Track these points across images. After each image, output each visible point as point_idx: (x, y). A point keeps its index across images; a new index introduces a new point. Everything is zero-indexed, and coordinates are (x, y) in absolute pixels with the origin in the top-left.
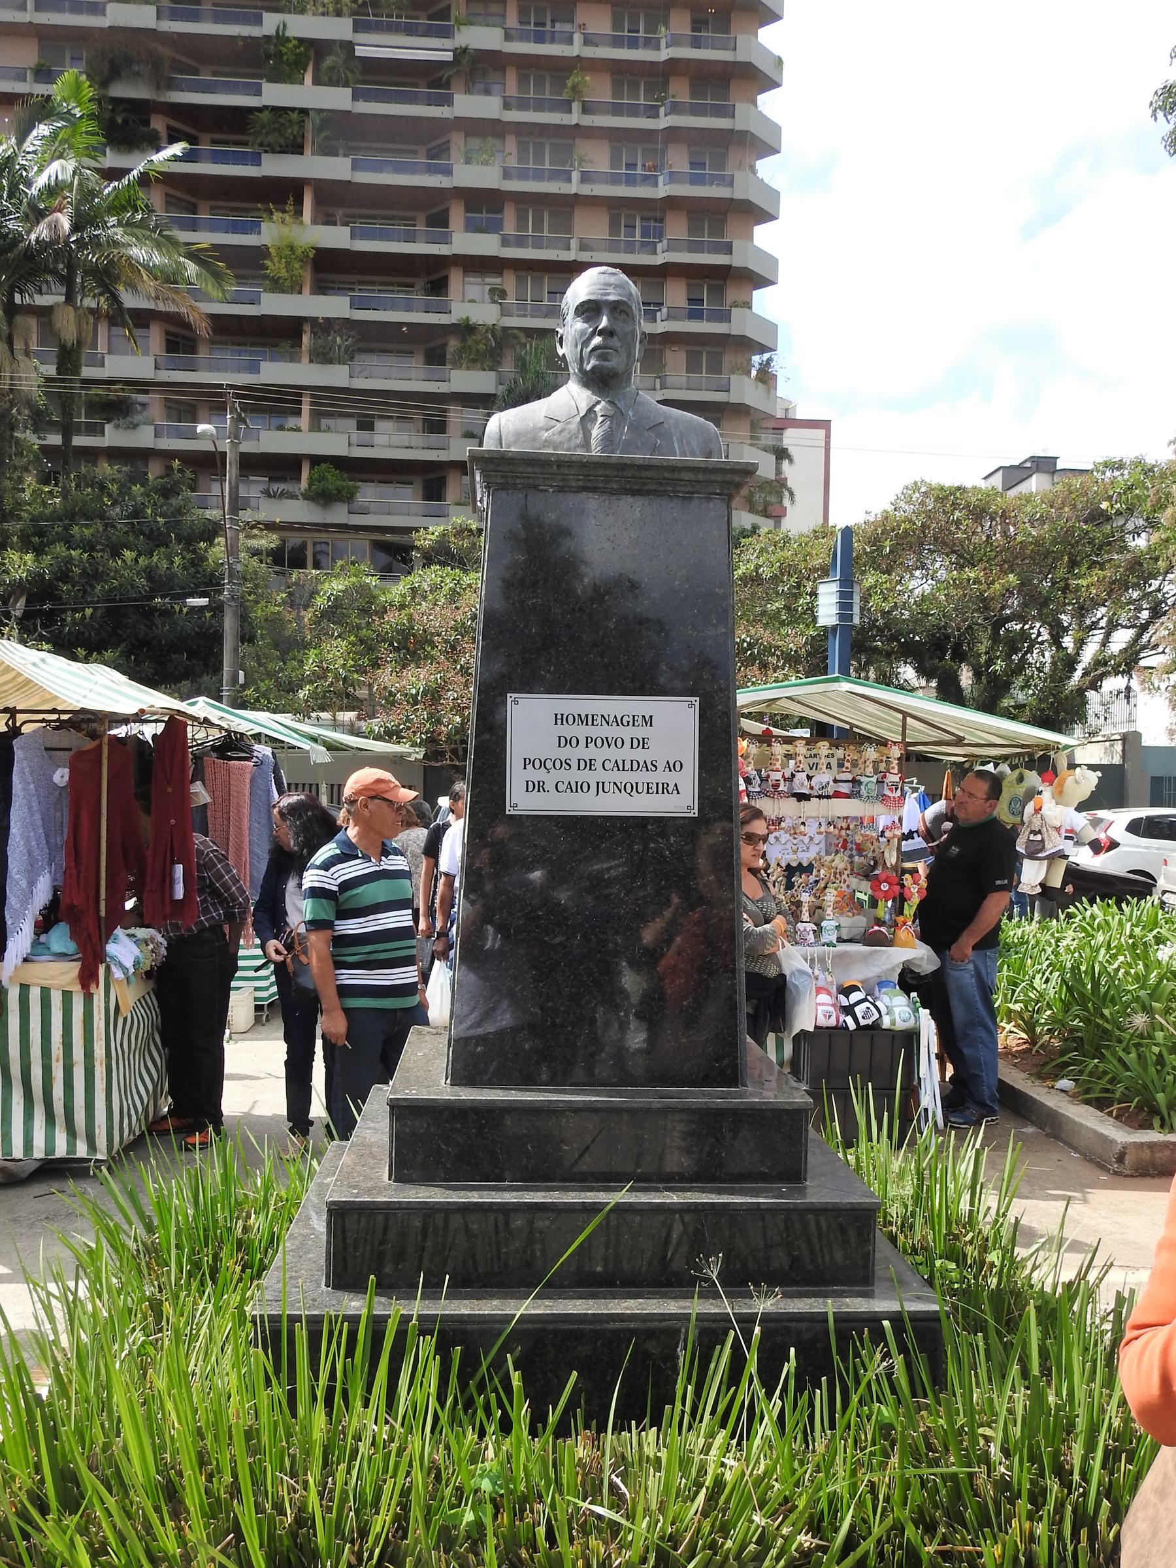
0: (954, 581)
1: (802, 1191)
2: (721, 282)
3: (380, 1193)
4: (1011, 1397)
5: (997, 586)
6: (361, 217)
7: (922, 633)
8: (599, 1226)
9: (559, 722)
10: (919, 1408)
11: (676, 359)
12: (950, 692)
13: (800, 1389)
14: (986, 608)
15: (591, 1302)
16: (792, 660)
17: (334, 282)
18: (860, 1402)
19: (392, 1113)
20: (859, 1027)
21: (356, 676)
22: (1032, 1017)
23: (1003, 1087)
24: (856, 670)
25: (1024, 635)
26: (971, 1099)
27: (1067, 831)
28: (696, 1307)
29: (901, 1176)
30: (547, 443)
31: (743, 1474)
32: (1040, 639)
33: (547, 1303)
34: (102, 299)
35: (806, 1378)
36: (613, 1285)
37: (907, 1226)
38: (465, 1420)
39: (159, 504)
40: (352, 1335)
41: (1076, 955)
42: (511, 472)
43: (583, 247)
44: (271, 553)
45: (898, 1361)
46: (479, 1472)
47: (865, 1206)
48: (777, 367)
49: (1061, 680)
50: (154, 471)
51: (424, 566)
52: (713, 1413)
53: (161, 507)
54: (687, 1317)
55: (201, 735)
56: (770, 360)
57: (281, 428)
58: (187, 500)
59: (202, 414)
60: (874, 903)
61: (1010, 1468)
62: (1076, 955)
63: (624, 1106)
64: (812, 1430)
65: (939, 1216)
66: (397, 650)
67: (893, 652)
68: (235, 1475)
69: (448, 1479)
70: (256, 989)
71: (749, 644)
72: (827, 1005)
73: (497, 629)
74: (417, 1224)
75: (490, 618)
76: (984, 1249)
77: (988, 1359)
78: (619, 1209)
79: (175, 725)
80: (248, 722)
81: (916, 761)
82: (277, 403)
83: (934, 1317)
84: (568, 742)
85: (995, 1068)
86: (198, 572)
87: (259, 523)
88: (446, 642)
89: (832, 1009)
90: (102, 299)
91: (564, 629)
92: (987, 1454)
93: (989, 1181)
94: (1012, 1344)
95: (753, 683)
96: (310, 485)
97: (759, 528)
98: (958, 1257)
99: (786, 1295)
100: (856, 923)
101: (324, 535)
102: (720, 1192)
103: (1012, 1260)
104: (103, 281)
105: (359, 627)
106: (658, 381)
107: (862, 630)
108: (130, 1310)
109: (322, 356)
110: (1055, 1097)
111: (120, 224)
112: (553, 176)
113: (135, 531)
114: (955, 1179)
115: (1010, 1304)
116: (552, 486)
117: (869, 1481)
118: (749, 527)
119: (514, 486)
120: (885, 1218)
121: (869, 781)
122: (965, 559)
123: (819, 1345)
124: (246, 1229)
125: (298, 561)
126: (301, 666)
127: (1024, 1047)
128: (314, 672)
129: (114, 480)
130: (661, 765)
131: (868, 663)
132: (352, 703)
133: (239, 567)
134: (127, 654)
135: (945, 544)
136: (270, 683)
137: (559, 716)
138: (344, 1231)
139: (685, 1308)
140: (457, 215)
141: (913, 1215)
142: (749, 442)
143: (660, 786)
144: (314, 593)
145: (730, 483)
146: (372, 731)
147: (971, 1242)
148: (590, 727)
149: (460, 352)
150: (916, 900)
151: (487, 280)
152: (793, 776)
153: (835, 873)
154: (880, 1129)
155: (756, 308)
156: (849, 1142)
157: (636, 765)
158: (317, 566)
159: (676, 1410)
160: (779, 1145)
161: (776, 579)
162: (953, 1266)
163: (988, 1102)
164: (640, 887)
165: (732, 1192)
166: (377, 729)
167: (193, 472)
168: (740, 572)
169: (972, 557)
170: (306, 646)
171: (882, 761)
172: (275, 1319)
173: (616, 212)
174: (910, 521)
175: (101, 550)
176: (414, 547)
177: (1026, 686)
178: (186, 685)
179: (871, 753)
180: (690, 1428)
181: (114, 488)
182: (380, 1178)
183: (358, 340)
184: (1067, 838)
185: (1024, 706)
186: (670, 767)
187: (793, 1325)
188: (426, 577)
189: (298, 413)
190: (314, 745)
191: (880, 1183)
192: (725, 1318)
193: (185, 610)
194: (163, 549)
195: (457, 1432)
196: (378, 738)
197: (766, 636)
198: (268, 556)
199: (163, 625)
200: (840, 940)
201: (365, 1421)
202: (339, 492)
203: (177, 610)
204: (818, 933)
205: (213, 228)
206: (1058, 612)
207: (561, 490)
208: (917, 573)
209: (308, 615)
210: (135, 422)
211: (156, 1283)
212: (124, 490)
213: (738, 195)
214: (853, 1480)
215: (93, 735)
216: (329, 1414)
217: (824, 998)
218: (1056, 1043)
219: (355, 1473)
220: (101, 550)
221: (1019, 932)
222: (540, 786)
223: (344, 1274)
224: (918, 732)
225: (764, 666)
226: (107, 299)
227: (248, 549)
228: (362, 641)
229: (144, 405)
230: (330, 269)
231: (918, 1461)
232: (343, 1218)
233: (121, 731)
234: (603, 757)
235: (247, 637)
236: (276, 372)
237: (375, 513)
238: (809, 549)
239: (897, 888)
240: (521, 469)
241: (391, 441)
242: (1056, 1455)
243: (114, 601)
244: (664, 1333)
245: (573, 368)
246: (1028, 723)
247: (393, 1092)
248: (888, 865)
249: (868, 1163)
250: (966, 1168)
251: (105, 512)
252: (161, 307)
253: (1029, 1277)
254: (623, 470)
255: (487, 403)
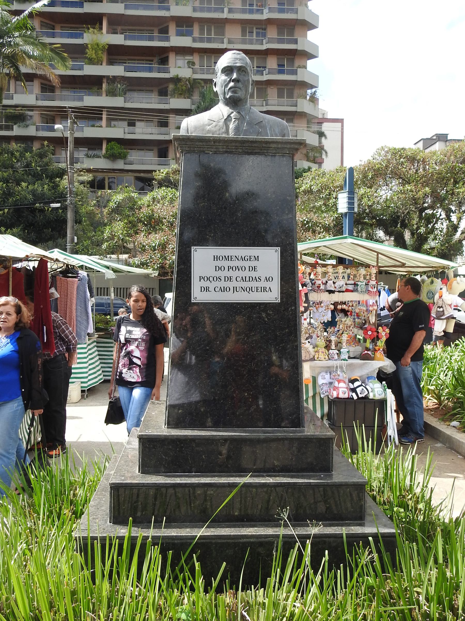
0: (401, 191)
1: (331, 476)
2: (292, 57)
3: (134, 479)
4: (429, 573)
5: (420, 192)
6: (129, 30)
7: (386, 215)
8: (236, 494)
9: (216, 259)
10: (387, 578)
11: (272, 92)
12: (400, 242)
13: (330, 570)
14: (416, 203)
15: (233, 529)
16: (327, 229)
17: (117, 60)
18: (359, 575)
19: (140, 442)
20: (359, 398)
21: (127, 238)
22: (439, 392)
23: (426, 425)
24: (357, 233)
25: (433, 216)
26: (412, 430)
27: (454, 306)
28: (281, 531)
29: (378, 468)
30: (209, 131)
31: (304, 611)
32: (441, 217)
33: (212, 530)
34: (12, 69)
35: (335, 563)
36: (243, 521)
37: (381, 492)
38: (174, 585)
39: (38, 161)
40: (121, 546)
41: (459, 363)
42: (194, 145)
43: (230, 42)
44: (89, 182)
45: (376, 556)
46: (180, 610)
47: (360, 483)
48: (318, 95)
49: (451, 236)
50: (36, 146)
51: (158, 188)
52: (290, 581)
53: (39, 162)
54: (278, 536)
55: (55, 266)
56: (315, 92)
57: (93, 126)
58: (51, 159)
59: (57, 120)
60: (365, 341)
61: (429, 607)
62: (459, 363)
63: (247, 437)
64: (336, 589)
65: (396, 487)
66: (146, 225)
67: (373, 224)
68: (66, 613)
69: (166, 613)
70: (82, 383)
71: (307, 222)
72: (344, 388)
73: (188, 218)
74: (152, 493)
75: (183, 213)
76: (417, 502)
77: (419, 554)
78: (246, 485)
79: (43, 262)
80: (76, 260)
81: (383, 274)
82: (92, 115)
83: (392, 536)
84: (220, 268)
85: (422, 416)
86: (56, 192)
87: (84, 169)
88: (169, 222)
89: (346, 390)
90: (12, 69)
91: (220, 215)
92: (418, 601)
93: (419, 470)
94: (430, 548)
95: (309, 240)
96: (107, 152)
97: (311, 168)
98: (406, 507)
99: (325, 526)
100: (357, 349)
101: (113, 174)
102: (292, 477)
103: (430, 508)
104: (11, 60)
105: (129, 216)
106: (264, 102)
107: (359, 214)
108: (20, 534)
109: (112, 93)
110: (450, 429)
111: (20, 36)
112: (216, 10)
113: (27, 173)
114: (403, 470)
115: (429, 528)
116: (211, 151)
117: (363, 614)
118: (307, 168)
119: (194, 152)
120: (371, 488)
121: (362, 284)
122: (405, 181)
123: (339, 549)
124: (74, 495)
125: (101, 186)
126: (103, 234)
127: (436, 406)
128: (108, 237)
129: (17, 150)
130: (263, 279)
131: (362, 229)
132: (126, 251)
133: (74, 189)
134: (23, 230)
135: (396, 175)
136: (89, 242)
137: (216, 257)
138: (118, 496)
139: (276, 532)
140: (172, 29)
141: (383, 487)
142: (306, 129)
143: (263, 288)
144: (109, 201)
145: (295, 147)
146: (135, 263)
147: (411, 499)
148: (230, 261)
149: (174, 90)
150: (384, 339)
151: (186, 58)
152: (327, 282)
153: (347, 327)
154: (368, 446)
155: (309, 68)
156: (354, 451)
157: (251, 279)
158: (110, 188)
159: (272, 580)
160: (318, 456)
161: (319, 191)
162: (402, 510)
163: (419, 432)
164: (253, 335)
165: (298, 477)
166: (137, 262)
167: (54, 147)
168: (303, 188)
169: (409, 180)
170: (105, 225)
171: (367, 275)
172: (85, 538)
173: (244, 26)
174: (381, 164)
175: (12, 183)
176: (154, 179)
177: (435, 239)
178: (50, 243)
179: (362, 271)
180: (279, 589)
181: (17, 154)
182: (134, 472)
183: (128, 86)
184: (454, 309)
185: (434, 248)
186: (267, 279)
187: (327, 539)
188: (159, 193)
189: (101, 119)
190: (108, 270)
191: (368, 471)
192: (292, 537)
193: (50, 209)
194: (39, 182)
195: (170, 591)
196: (138, 266)
197: (314, 217)
198: (88, 184)
199: (40, 216)
200: (349, 358)
201: (127, 586)
202: (120, 154)
203: (47, 209)
204: (339, 354)
205: (62, 36)
206: (449, 204)
207: (215, 153)
208: (384, 188)
209: (105, 211)
210: (27, 124)
211: (33, 521)
212: (22, 155)
213: (300, 17)
214: (355, 613)
215: (5, 268)
216: (111, 583)
217: (342, 385)
218: (450, 404)
219: (122, 611)
220: (12, 183)
221: (433, 353)
222: (207, 289)
223: (118, 518)
224: (384, 261)
225: (314, 232)
226: (14, 69)
227: (79, 181)
228: (130, 222)
229: (31, 116)
230: (115, 54)
231: (386, 603)
232: (118, 490)
233: (19, 265)
234: (235, 275)
235: (78, 221)
236: (90, 101)
237: (136, 164)
238: (334, 178)
239: (375, 334)
240: (197, 144)
241: (144, 131)
242: (451, 601)
243: (18, 205)
244: (266, 544)
245: (221, 97)
246: (436, 256)
247: (140, 432)
248: (371, 323)
249: (362, 462)
250: (408, 464)
251: (13, 165)
252: (38, 72)
253: (438, 515)
254: (244, 143)
255: (187, 113)
